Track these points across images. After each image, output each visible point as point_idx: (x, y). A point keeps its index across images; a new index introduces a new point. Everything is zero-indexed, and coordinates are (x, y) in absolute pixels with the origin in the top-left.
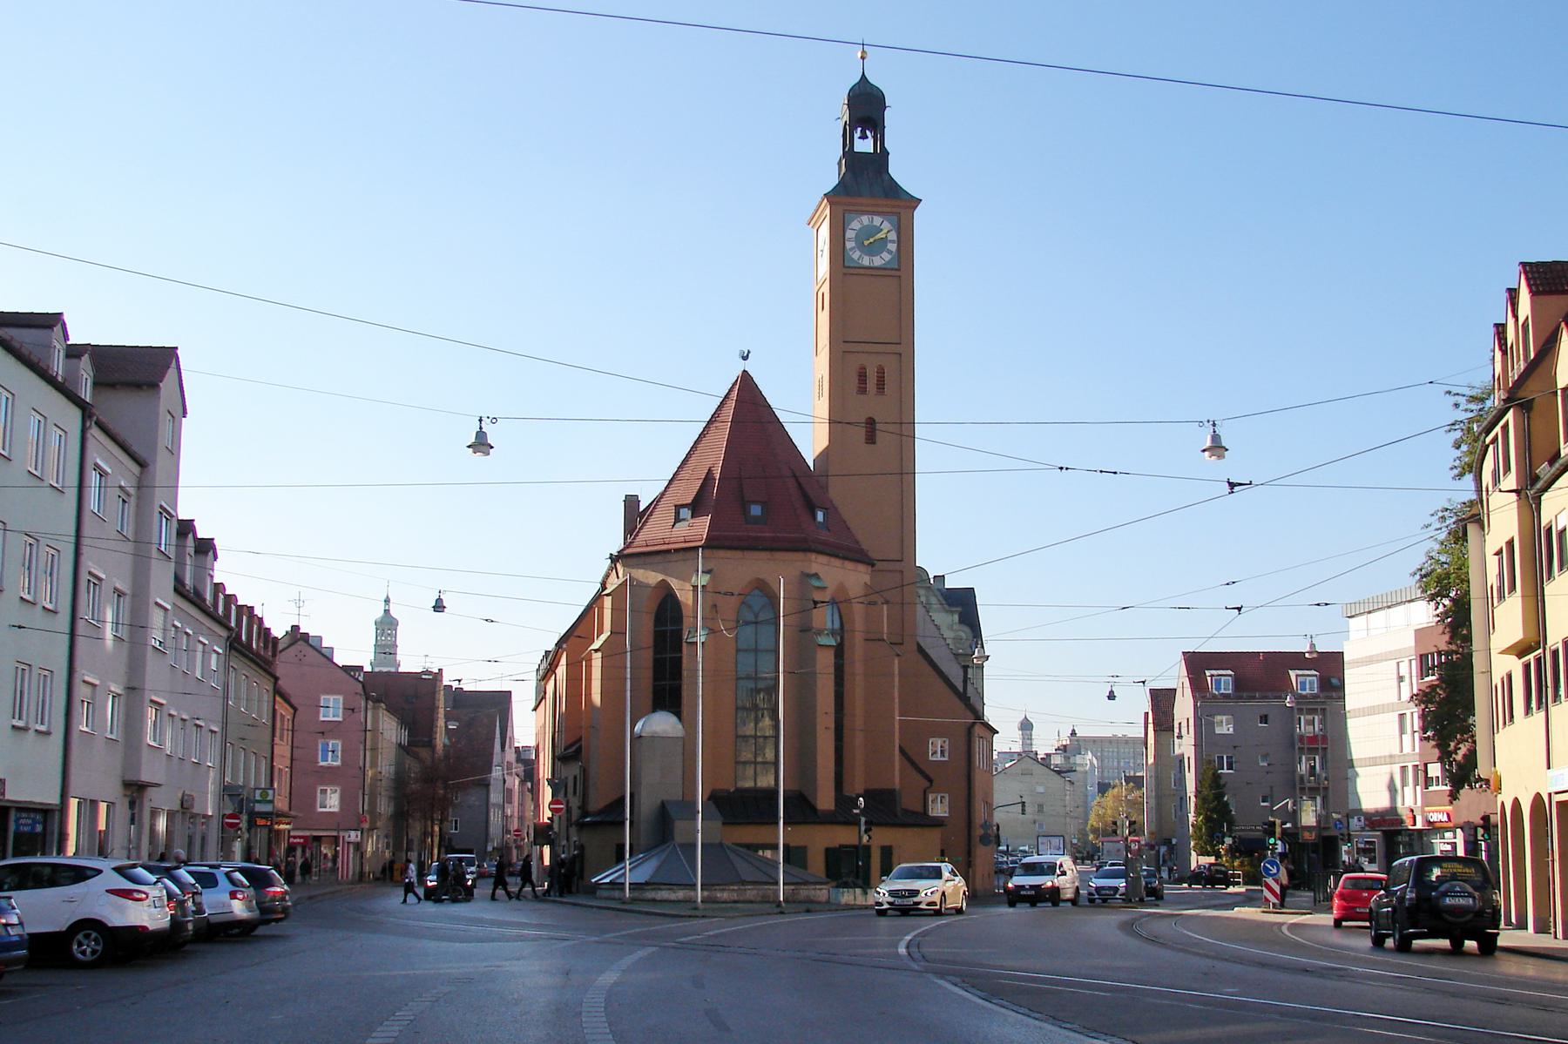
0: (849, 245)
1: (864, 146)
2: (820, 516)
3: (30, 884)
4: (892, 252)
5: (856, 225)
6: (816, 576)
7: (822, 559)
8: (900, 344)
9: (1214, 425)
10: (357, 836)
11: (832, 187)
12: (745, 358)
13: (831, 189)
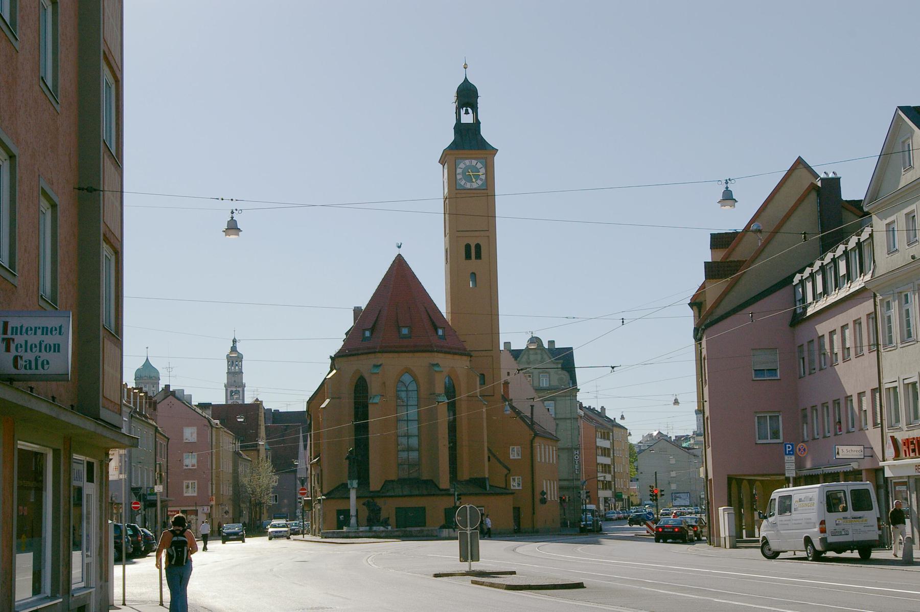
0: (459, 177)
1: (467, 119)
2: (440, 332)
3: (802, 484)
4: (483, 179)
5: (462, 165)
6: (437, 365)
7: (441, 355)
8: (488, 231)
9: (532, 333)
10: (208, 510)
11: (449, 145)
12: (399, 247)
13: (447, 146)
